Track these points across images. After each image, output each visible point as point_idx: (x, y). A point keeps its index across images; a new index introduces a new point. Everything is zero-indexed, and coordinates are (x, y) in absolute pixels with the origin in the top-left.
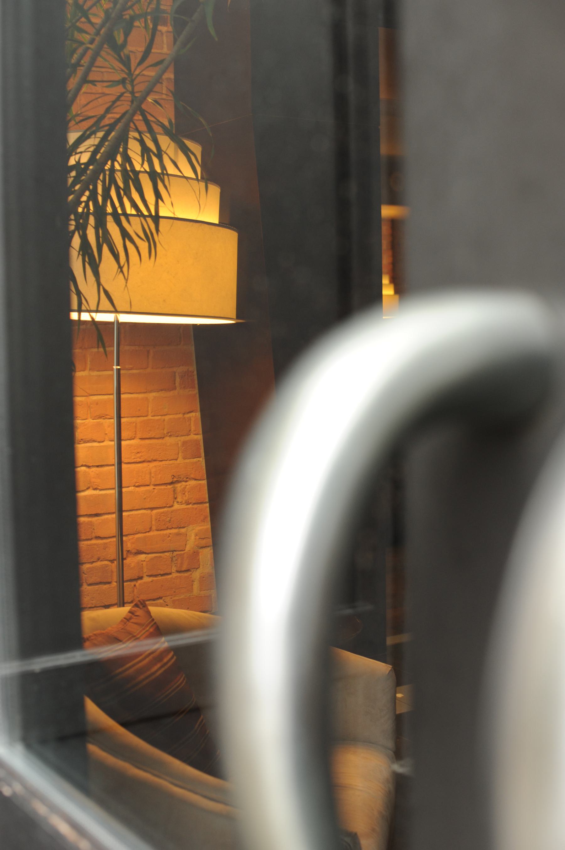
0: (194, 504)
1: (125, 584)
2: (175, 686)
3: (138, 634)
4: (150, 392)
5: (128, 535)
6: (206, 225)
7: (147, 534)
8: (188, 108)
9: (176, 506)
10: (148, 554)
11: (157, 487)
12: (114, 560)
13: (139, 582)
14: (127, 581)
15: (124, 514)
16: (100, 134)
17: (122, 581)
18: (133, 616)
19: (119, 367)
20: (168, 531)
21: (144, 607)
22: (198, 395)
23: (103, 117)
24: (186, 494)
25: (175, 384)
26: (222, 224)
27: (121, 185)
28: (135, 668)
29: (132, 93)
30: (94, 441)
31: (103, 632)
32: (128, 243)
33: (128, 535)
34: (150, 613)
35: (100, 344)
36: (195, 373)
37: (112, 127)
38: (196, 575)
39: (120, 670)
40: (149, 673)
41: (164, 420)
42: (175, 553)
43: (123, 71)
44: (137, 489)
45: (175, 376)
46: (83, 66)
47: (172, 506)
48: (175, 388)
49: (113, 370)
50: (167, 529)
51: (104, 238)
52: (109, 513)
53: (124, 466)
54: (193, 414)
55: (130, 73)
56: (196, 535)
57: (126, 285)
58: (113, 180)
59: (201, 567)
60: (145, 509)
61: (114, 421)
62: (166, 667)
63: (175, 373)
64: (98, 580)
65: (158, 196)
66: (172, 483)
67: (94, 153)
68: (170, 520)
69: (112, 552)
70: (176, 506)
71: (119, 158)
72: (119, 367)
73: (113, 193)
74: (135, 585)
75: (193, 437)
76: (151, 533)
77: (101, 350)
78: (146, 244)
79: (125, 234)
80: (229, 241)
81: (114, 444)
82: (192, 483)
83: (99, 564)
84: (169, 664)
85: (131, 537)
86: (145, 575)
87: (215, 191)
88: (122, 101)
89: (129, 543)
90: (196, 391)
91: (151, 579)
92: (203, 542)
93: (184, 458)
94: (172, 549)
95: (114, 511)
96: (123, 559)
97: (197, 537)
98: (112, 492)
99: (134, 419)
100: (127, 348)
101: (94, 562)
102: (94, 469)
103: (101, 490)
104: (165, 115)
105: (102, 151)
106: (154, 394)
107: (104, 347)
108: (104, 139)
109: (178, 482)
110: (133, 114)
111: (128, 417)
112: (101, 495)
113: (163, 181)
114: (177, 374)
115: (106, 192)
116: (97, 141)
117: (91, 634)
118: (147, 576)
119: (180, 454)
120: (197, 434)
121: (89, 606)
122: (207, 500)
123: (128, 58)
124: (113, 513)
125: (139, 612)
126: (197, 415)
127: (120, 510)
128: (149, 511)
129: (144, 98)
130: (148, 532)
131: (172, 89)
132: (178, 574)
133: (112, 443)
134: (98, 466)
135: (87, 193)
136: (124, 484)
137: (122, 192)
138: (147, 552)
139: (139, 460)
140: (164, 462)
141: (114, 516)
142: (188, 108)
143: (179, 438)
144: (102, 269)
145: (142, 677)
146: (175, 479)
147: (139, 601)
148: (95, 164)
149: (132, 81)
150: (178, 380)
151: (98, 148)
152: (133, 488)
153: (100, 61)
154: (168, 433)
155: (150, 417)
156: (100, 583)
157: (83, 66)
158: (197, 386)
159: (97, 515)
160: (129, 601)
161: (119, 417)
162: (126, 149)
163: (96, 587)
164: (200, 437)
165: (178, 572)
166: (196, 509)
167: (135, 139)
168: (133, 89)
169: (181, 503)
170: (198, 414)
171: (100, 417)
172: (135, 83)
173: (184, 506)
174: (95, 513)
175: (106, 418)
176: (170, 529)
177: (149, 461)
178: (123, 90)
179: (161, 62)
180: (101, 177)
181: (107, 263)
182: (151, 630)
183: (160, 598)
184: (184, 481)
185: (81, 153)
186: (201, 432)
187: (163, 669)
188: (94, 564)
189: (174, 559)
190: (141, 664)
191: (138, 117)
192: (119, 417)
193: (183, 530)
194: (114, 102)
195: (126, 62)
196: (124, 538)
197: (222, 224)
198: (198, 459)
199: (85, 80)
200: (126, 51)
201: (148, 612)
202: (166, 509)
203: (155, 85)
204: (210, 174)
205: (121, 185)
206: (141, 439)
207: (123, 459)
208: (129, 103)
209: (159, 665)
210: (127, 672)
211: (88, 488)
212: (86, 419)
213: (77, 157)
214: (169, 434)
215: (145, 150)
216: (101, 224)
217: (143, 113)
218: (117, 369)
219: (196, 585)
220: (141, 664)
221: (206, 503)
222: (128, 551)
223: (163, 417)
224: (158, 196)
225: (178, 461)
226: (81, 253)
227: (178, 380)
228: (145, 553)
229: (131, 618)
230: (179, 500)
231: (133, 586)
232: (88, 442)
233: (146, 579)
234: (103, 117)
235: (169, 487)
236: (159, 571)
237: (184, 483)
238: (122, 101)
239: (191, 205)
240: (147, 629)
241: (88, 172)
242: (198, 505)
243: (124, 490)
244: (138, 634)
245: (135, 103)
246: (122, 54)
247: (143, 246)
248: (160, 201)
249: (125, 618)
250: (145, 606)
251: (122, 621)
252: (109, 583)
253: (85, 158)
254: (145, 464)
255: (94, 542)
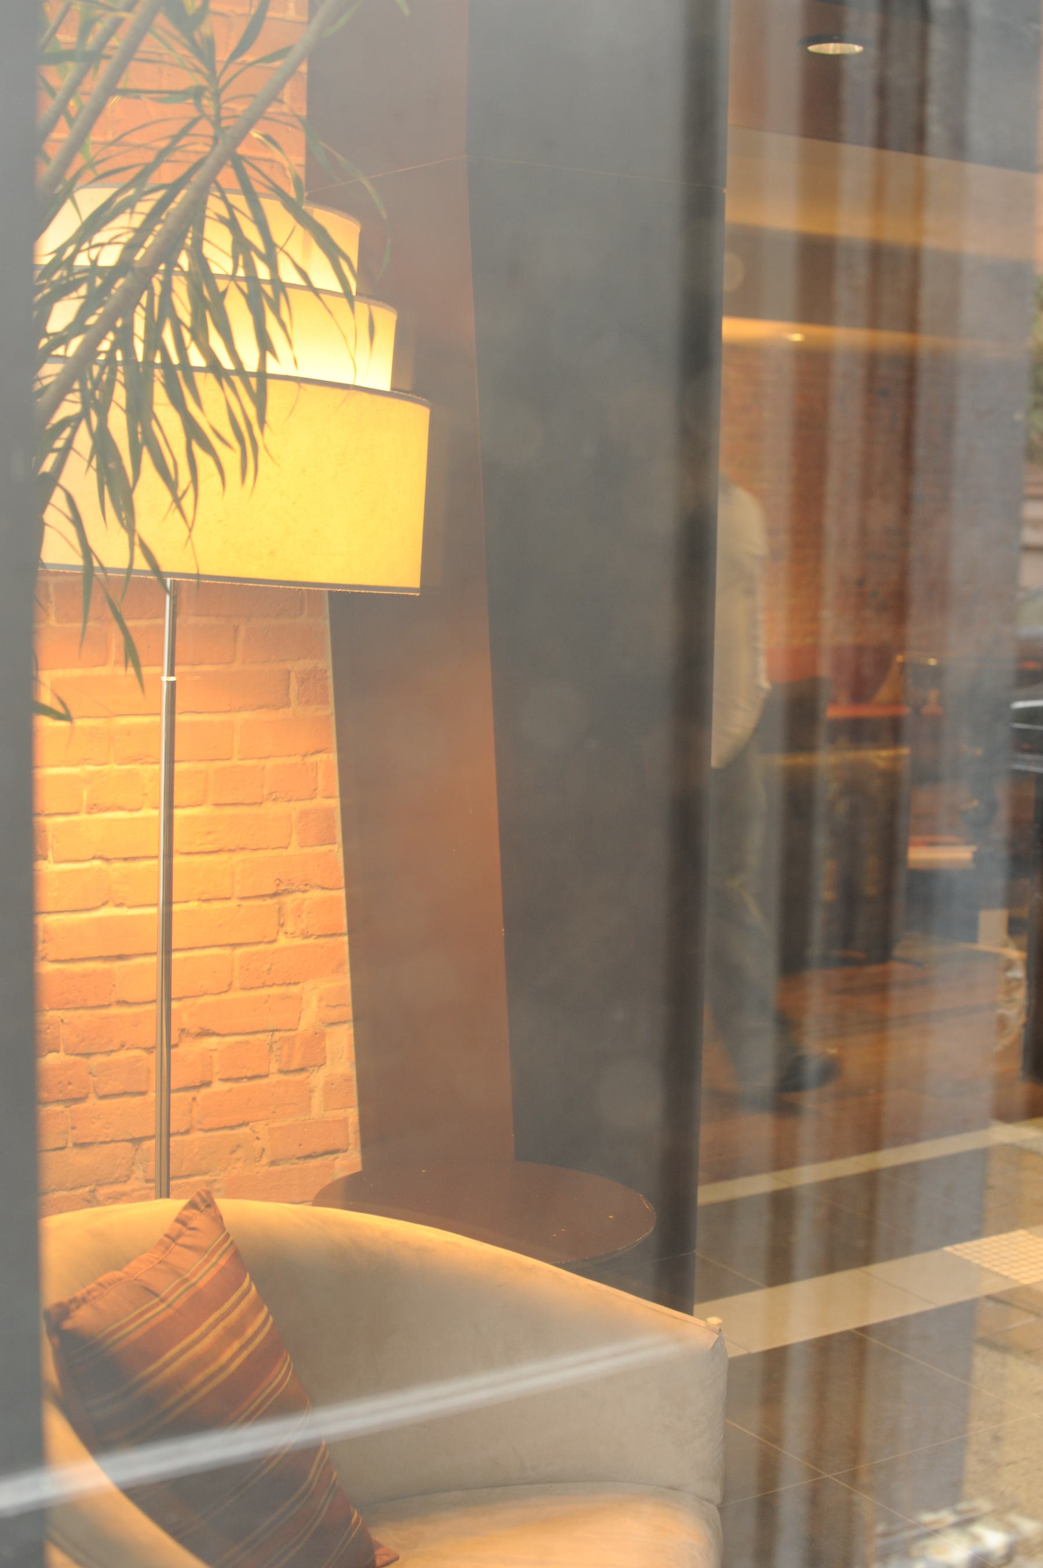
0: (319, 936)
1: (173, 1096)
2: (268, 1391)
3: (194, 1275)
4: (239, 710)
5: (184, 997)
6: (365, 395)
7: (223, 997)
8: (339, 156)
9: (283, 941)
10: (224, 1035)
11: (246, 903)
12: (153, 1048)
13: (204, 1091)
14: (179, 1090)
15: (175, 956)
16: (145, 207)
17: (166, 1089)
18: (184, 1229)
19: (173, 679)
20: (265, 992)
21: (208, 1206)
22: (333, 719)
23: (147, 170)
24: (304, 916)
25: (288, 694)
26: (397, 392)
27: (186, 317)
28: (185, 1357)
29: (217, 121)
30: (121, 808)
31: (119, 1274)
32: (197, 449)
33: (184, 997)
34: (221, 1218)
35: (130, 663)
36: (330, 673)
37: (173, 189)
38: (318, 1078)
39: (152, 1368)
40: (213, 1367)
41: (264, 768)
42: (278, 1035)
43: (197, 70)
44: (205, 905)
45: (289, 679)
46: (108, 57)
47: (274, 941)
48: (288, 704)
49: (161, 682)
50: (264, 986)
51: (144, 439)
52: (146, 954)
53: (177, 860)
54: (323, 756)
55: (213, 76)
56: (321, 999)
57: (189, 537)
58: (167, 308)
59: (328, 1062)
60: (220, 946)
61: (161, 768)
62: (251, 1348)
63: (289, 673)
64: (120, 1088)
65: (265, 344)
66: (275, 895)
67: (131, 247)
68: (269, 970)
69: (149, 1032)
70: (283, 941)
71: (184, 260)
72: (173, 679)
73: (168, 336)
74: (194, 1099)
75: (320, 802)
76: (231, 996)
77: (131, 670)
78: (237, 456)
79: (193, 431)
80: (411, 426)
81: (158, 814)
82: (316, 894)
83: (123, 1055)
84: (258, 1340)
85: (188, 1002)
86: (215, 1079)
87: (386, 320)
88: (193, 135)
89: (183, 1013)
90: (330, 710)
91: (228, 1085)
92: (334, 1014)
93: (302, 845)
94: (270, 1028)
95: (154, 950)
96: (169, 1047)
97: (323, 1004)
98: (153, 910)
99: (202, 766)
100: (192, 620)
101: (112, 1051)
102: (117, 865)
103: (130, 907)
104: (289, 160)
105: (148, 244)
106: (246, 715)
107: (137, 666)
108: (153, 217)
109: (287, 892)
110: (219, 166)
111: (189, 761)
112: (132, 917)
113: (277, 312)
114: (293, 675)
115: (154, 342)
116: (137, 221)
117: (93, 1285)
118: (221, 1080)
119: (294, 837)
120: (330, 797)
121: (100, 1139)
122: (345, 930)
123: (210, 43)
124: (155, 954)
125: (199, 1220)
126: (332, 758)
127: (167, 949)
128: (227, 951)
129: (243, 134)
130: (226, 992)
131: (304, 113)
132: (283, 1077)
133: (155, 813)
134: (126, 859)
135: (111, 336)
136: (175, 897)
137: (187, 336)
138: (222, 1032)
139: (210, 847)
140: (261, 854)
141: (154, 959)
142: (339, 156)
143: (292, 804)
144: (140, 498)
145: (199, 1378)
146: (282, 887)
147: (199, 1194)
148: (130, 275)
149: (217, 95)
150: (294, 687)
151: (142, 233)
152: (196, 903)
153: (149, 45)
154: (271, 794)
155: (235, 762)
156: (124, 1094)
157: (108, 57)
158: (332, 699)
159: (120, 957)
160: (183, 1130)
161: (171, 761)
162: (199, 241)
163: (116, 1102)
164: (335, 803)
165: (281, 1071)
166: (323, 947)
167: (221, 220)
168: (219, 109)
169: (293, 935)
170: (333, 757)
171: (134, 760)
172: (224, 96)
173: (299, 941)
174: (117, 953)
175: (147, 763)
176: (270, 986)
177: (231, 851)
178: (193, 113)
179: (281, 54)
180: (144, 300)
181: (149, 492)
182: (223, 1262)
183: (244, 1124)
184: (299, 891)
185: (102, 245)
186: (337, 792)
187: (245, 1354)
188: (114, 1057)
189: (275, 1047)
190: (198, 1348)
191: (227, 177)
192: (171, 761)
193: (294, 990)
194: (177, 138)
195: (205, 51)
196: (174, 1005)
197: (397, 392)
198: (330, 847)
199: (111, 89)
200: (205, 29)
201: (218, 1218)
202: (261, 947)
203: (267, 104)
204: (378, 279)
205: (186, 317)
206: (217, 805)
207: (176, 845)
208: (210, 141)
209: (236, 1345)
210: (168, 1371)
211: (104, 904)
212: (105, 764)
213: (93, 253)
214: (274, 796)
215: (241, 246)
216: (139, 411)
217: (238, 164)
218: (168, 682)
219: (317, 1099)
220: (198, 1348)
221: (341, 934)
222: (183, 1030)
223: (262, 762)
224: (265, 344)
225: (290, 851)
226: (94, 463)
227: (294, 687)
228: (219, 1035)
229: (180, 1235)
230: (289, 928)
231: (190, 1099)
232: (108, 809)
233: (218, 1086)
234: (147, 170)
235: (270, 902)
236: (245, 1070)
237: (299, 895)
238: (193, 135)
239: (338, 347)
240: (214, 1259)
241: (113, 291)
242: (327, 940)
243: (176, 908)
244: (194, 1275)
245: (220, 142)
246: (197, 37)
247: (230, 458)
248: (269, 356)
249: (167, 1236)
250: (210, 1204)
251: (161, 1242)
252: (143, 1093)
253: (109, 257)
254: (223, 857)
255: (114, 1011)
